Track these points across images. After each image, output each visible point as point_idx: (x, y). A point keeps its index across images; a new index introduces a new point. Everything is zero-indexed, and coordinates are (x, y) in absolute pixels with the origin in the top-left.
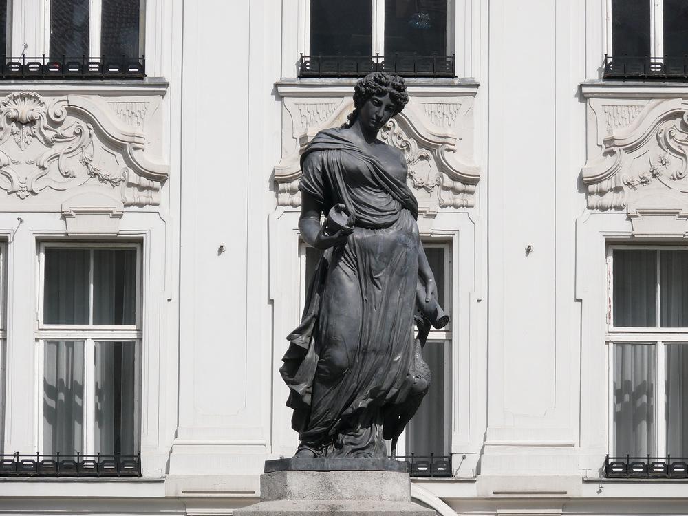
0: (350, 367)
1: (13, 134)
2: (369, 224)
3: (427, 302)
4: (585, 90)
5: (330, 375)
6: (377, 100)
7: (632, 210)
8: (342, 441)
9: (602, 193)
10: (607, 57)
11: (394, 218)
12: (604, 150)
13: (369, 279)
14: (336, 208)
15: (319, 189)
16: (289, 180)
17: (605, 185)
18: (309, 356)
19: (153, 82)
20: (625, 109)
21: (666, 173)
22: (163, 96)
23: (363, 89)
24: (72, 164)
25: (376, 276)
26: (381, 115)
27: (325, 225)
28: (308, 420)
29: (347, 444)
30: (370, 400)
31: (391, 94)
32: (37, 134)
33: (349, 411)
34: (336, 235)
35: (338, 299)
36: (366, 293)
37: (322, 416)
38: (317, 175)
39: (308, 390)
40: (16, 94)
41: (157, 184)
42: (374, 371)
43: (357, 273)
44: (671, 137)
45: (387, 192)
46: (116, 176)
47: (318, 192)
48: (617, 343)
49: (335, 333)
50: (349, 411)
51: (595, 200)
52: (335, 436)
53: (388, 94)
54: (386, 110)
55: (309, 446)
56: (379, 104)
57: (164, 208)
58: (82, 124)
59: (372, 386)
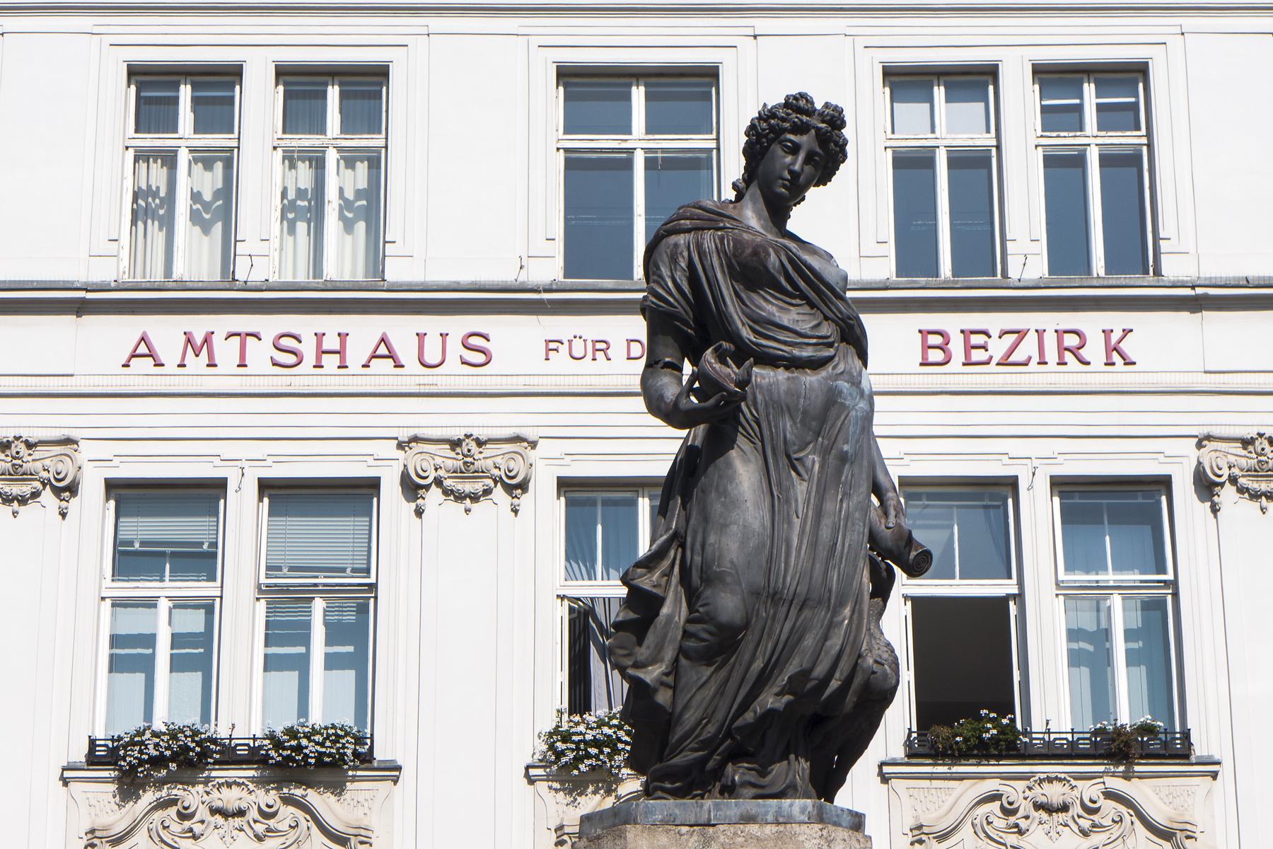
0: (746, 626)
1: (216, 827)
2: (783, 358)
3: (888, 528)
4: (886, 769)
5: (717, 643)
6: (791, 141)
8: (733, 780)
10: (910, 732)
11: (831, 352)
12: (910, 839)
13: (784, 461)
14: (716, 350)
15: (683, 302)
18: (665, 610)
19: (383, 765)
20: (933, 791)
22: (395, 782)
23: (764, 125)
25: (796, 456)
26: (797, 167)
27: (691, 382)
28: (664, 744)
30: (788, 698)
31: (818, 129)
32: (246, 827)
33: (749, 717)
34: (712, 401)
35: (725, 493)
36: (780, 484)
37: (693, 730)
38: (678, 275)
39: (665, 678)
40: (221, 781)
42: (797, 636)
43: (760, 448)
44: (989, 823)
45: (812, 305)
47: (682, 308)
49: (720, 558)
50: (749, 717)
52: (718, 773)
53: (813, 131)
56: (794, 150)
58: (300, 814)
59: (792, 668)
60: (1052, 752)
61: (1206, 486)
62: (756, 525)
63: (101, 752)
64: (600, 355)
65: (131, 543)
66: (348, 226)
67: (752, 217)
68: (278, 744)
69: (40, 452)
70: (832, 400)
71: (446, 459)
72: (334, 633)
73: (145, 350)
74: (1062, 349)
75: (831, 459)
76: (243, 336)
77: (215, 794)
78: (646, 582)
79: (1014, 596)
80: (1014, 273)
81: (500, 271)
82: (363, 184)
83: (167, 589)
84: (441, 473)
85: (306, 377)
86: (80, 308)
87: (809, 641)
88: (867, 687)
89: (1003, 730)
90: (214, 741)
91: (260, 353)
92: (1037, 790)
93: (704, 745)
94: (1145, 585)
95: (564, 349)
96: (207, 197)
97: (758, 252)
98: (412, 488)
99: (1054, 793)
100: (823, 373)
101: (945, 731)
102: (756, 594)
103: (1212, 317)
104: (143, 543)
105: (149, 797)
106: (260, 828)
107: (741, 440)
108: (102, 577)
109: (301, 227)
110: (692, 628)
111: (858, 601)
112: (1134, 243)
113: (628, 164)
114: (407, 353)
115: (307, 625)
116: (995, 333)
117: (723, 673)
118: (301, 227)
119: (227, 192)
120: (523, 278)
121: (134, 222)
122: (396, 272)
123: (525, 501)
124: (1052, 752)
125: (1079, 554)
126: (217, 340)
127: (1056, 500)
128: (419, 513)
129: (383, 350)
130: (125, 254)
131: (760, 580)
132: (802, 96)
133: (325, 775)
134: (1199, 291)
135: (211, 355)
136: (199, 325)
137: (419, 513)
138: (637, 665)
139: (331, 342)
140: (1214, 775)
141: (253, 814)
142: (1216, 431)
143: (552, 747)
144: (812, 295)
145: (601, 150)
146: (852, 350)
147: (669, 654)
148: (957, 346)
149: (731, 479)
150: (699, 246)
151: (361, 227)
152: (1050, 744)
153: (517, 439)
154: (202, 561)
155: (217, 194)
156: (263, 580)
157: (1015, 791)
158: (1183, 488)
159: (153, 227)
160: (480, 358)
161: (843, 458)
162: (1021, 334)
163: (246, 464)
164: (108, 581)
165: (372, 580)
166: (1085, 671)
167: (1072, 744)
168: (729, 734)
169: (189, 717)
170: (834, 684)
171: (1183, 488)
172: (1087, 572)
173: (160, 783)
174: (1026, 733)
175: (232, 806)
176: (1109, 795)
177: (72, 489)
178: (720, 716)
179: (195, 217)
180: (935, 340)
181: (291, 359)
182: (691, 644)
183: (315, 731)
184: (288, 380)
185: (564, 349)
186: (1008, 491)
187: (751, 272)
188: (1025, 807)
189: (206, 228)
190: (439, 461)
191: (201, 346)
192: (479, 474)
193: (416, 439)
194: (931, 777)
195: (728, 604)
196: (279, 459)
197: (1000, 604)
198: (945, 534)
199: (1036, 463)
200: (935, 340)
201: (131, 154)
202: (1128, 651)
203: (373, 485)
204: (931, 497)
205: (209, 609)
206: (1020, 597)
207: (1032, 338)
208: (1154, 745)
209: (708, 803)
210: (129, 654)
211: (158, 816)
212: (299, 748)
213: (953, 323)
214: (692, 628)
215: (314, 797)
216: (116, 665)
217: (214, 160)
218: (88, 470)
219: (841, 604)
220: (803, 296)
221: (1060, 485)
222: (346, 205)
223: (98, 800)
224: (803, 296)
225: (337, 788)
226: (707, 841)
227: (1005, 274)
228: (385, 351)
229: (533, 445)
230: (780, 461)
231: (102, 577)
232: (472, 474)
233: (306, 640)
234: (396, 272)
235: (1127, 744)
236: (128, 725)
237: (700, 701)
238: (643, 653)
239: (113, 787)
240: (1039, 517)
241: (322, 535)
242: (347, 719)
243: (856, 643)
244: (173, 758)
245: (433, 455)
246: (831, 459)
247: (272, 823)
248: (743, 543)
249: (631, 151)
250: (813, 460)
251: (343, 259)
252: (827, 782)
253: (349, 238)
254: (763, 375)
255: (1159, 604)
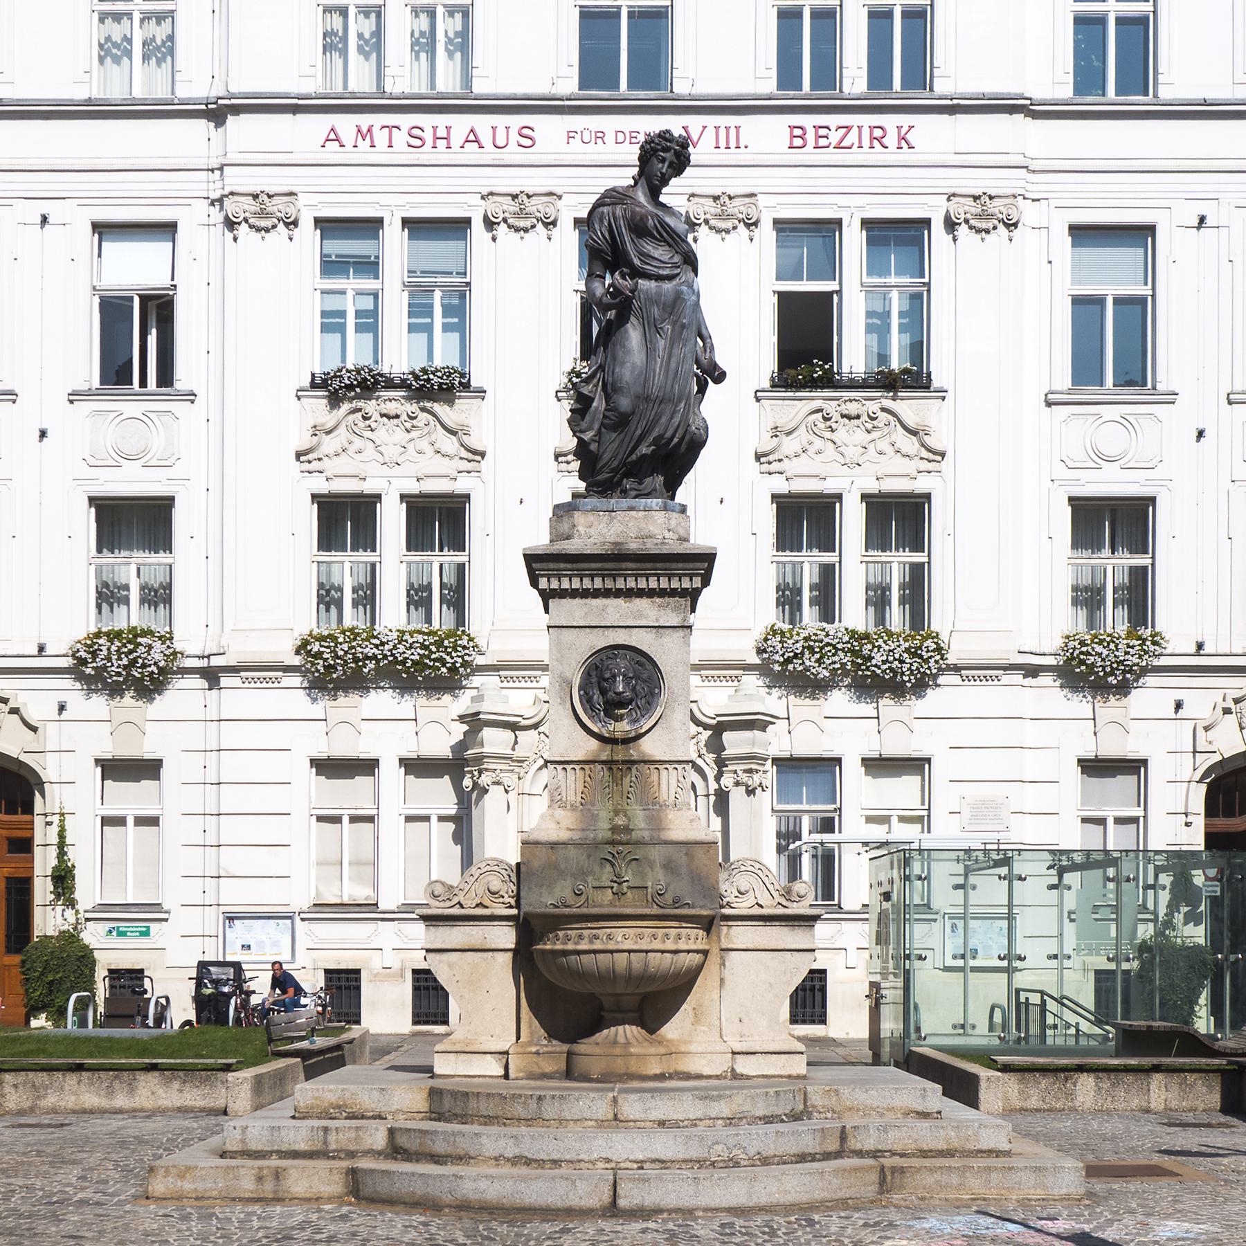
0: (633, 413)
5: (618, 422)
7: (789, 474)
9: (770, 463)
16: (565, 455)
17: (771, 458)
18: (595, 404)
21: (812, 450)
24: (424, 444)
28: (594, 467)
29: (632, 489)
33: (634, 457)
35: (624, 346)
41: (479, 458)
45: (670, 246)
46: (451, 451)
47: (605, 247)
48: (778, 563)
50: (634, 457)
51: (765, 467)
52: (619, 483)
54: (669, 167)
55: (597, 492)
56: (663, 160)
57: (483, 475)
58: (430, 417)
59: (655, 433)
60: (853, 385)
61: (951, 225)
62: (639, 363)
63: (318, 381)
64: (599, 141)
65: (330, 256)
66: (451, 55)
67: (641, 196)
68: (417, 378)
69: (276, 200)
70: (678, 296)
71: (509, 206)
72: (447, 310)
73: (334, 137)
74: (872, 138)
75: (677, 328)
76: (390, 128)
77: (383, 405)
78: (586, 390)
79: (836, 292)
80: (846, 89)
81: (539, 86)
82: (459, 28)
83: (352, 283)
84: (507, 215)
85: (427, 154)
86: (295, 110)
87: (664, 420)
88: (692, 441)
89: (825, 371)
90: (381, 375)
91: (400, 138)
92: (843, 406)
93: (612, 470)
94: (912, 285)
95: (578, 136)
96: (367, 36)
97: (643, 219)
98: (490, 224)
99: (852, 408)
100: (674, 283)
101: (792, 372)
102: (638, 397)
103: (961, 118)
104: (337, 256)
105: (346, 407)
106: (408, 425)
107: (632, 318)
108: (314, 277)
109: (423, 56)
110: (608, 414)
111: (688, 398)
112: (919, 71)
113: (617, 15)
114: (486, 139)
115: (432, 306)
116: (833, 128)
117: (622, 436)
118: (423, 56)
119: (378, 33)
120: (554, 91)
121: (324, 53)
122: (479, 87)
123: (555, 232)
124: (853, 385)
125: (875, 266)
126: (375, 130)
127: (864, 232)
128: (494, 239)
129: (472, 137)
130: (319, 75)
131: (640, 391)
132: (668, 131)
133: (444, 395)
134: (955, 102)
135: (372, 140)
136: (365, 120)
137: (494, 239)
138: (581, 432)
139: (442, 132)
140: (943, 398)
141: (404, 417)
142: (958, 191)
143: (570, 380)
144: (670, 240)
145: (601, 7)
146: (690, 268)
147: (596, 426)
148: (810, 136)
149: (627, 339)
150: (614, 214)
151: (458, 55)
152: (851, 380)
153: (551, 194)
154: (370, 267)
155: (373, 34)
156: (406, 279)
157: (831, 407)
158: (938, 226)
159: (336, 55)
160: (529, 142)
161: (683, 326)
162: (849, 128)
163: (394, 209)
164: (318, 279)
165: (467, 280)
166: (875, 336)
167: (864, 380)
168: (624, 465)
169: (367, 361)
170: (676, 440)
171: (938, 226)
172: (880, 276)
173: (351, 399)
174: (838, 373)
175: (392, 413)
176: (883, 409)
177: (295, 223)
178: (620, 457)
179: (360, 50)
180: (798, 132)
181: (419, 143)
182: (607, 421)
183: (437, 371)
184: (417, 156)
185: (578, 136)
186: (837, 226)
187: (640, 229)
188: (836, 416)
189: (367, 58)
190: (505, 207)
191: (365, 134)
192: (528, 215)
193: (491, 194)
194: (784, 399)
195: (624, 403)
196: (414, 205)
197: (828, 296)
198: (795, 251)
199: (854, 210)
200: (798, 132)
201: (321, 8)
202: (900, 325)
203: (467, 222)
204: (792, 230)
205: (376, 296)
206: (839, 292)
207: (855, 131)
208: (913, 379)
209: (613, 501)
210: (332, 322)
211: (351, 417)
212: (429, 380)
213: (808, 121)
214: (608, 414)
215: (437, 408)
216: (325, 328)
217: (370, 12)
218: (303, 210)
219: (680, 401)
220: (665, 241)
221: (867, 223)
222: (449, 41)
223: (318, 404)
224: (665, 241)
225: (450, 402)
226: (612, 519)
227: (841, 91)
228: (473, 138)
229: (560, 197)
230: (651, 328)
231: (314, 277)
232: (524, 215)
233: (430, 314)
234: (479, 87)
235: (895, 380)
236: (332, 365)
237: (611, 449)
238: (584, 425)
239: (325, 401)
240: (853, 243)
241: (439, 251)
242: (455, 363)
243: (687, 419)
244: (358, 386)
245: (501, 204)
246: (677, 328)
247: (414, 422)
248: (632, 372)
249: (619, 7)
250: (668, 327)
251: (448, 80)
252: (672, 486)
253: (451, 63)
254: (643, 284)
255: (920, 296)
